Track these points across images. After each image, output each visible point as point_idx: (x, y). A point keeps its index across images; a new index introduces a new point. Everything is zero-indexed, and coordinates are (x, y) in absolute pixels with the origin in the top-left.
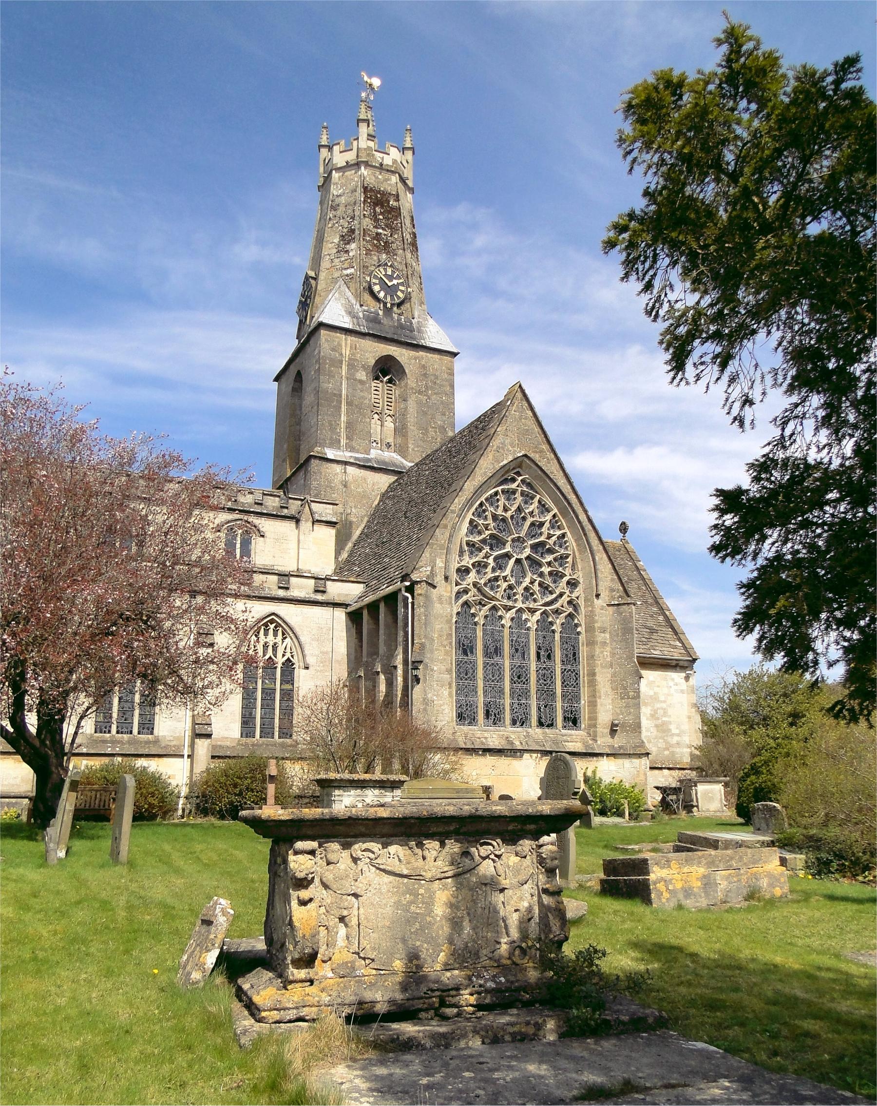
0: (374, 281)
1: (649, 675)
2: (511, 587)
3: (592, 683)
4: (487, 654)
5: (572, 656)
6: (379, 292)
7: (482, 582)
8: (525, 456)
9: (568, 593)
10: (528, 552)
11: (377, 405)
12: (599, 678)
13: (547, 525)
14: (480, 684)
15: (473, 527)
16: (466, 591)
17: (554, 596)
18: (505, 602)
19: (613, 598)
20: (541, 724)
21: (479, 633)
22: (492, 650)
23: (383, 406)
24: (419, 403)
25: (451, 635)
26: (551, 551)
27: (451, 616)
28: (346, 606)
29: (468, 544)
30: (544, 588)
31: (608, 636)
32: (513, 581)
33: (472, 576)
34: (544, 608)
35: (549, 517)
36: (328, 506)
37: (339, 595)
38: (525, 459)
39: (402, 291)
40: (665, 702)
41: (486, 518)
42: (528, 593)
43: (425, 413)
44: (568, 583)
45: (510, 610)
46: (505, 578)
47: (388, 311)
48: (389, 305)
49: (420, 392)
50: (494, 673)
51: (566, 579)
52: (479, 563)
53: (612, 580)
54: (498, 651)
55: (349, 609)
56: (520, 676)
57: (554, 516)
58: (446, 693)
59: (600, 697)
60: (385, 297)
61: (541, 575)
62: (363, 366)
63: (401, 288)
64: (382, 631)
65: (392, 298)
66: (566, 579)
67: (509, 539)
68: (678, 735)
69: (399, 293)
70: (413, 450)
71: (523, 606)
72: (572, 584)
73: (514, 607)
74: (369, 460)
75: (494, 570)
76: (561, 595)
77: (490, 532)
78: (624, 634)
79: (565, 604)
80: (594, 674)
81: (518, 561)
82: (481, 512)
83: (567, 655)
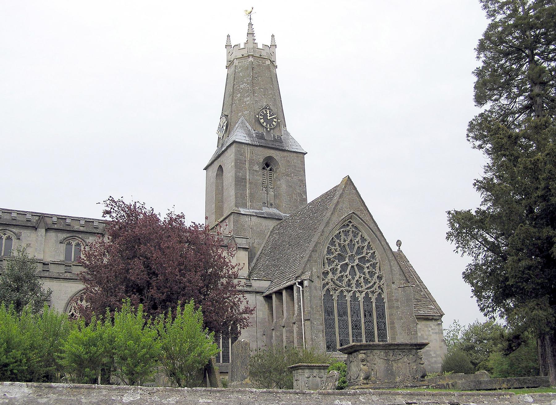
0: (261, 117)
1: (421, 325)
2: (349, 280)
3: (393, 328)
4: (339, 315)
5: (381, 316)
6: (263, 123)
7: (335, 278)
8: (353, 213)
9: (378, 282)
10: (357, 262)
11: (265, 183)
12: (396, 325)
13: (366, 248)
15: (329, 252)
16: (327, 284)
17: (371, 284)
18: (347, 288)
19: (401, 284)
21: (335, 305)
23: (268, 183)
25: (322, 306)
26: (368, 261)
27: (322, 296)
28: (263, 293)
30: (366, 281)
31: (399, 303)
32: (350, 277)
33: (330, 275)
34: (367, 290)
35: (366, 244)
36: (244, 239)
37: (258, 287)
38: (354, 214)
40: (427, 339)
41: (335, 246)
42: (358, 284)
43: (291, 187)
44: (378, 277)
45: (350, 292)
46: (346, 276)
47: (268, 132)
48: (269, 129)
49: (287, 175)
51: (376, 275)
52: (333, 268)
53: (400, 275)
54: (345, 313)
55: (264, 294)
56: (356, 326)
57: (369, 243)
58: (321, 335)
61: (364, 273)
62: (257, 163)
63: (275, 120)
64: (285, 306)
65: (270, 126)
66: (376, 275)
67: (348, 256)
68: (435, 357)
69: (274, 123)
70: (285, 206)
71: (356, 290)
72: (380, 278)
73: (352, 290)
74: (263, 213)
75: (341, 272)
76: (375, 283)
77: (338, 253)
78: (407, 302)
79: (377, 288)
80: (394, 323)
81: (352, 267)
82: (333, 243)
83: (379, 314)
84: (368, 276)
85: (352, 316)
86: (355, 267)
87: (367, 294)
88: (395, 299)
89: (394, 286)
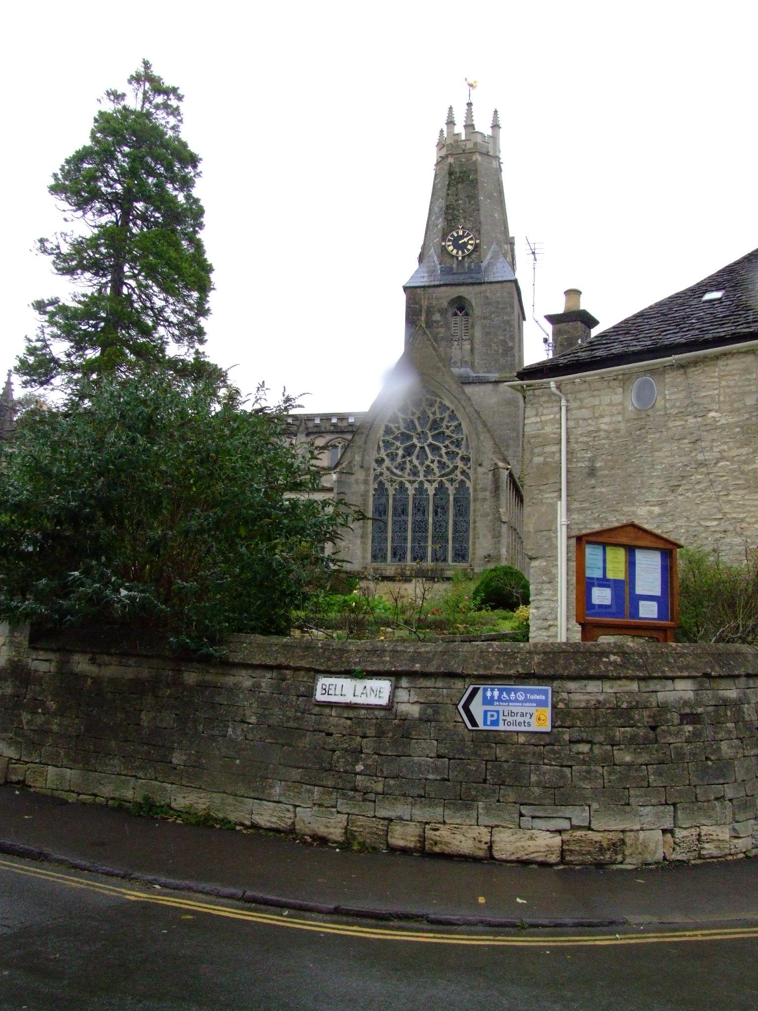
0: (448, 243)
6: (452, 251)
14: (390, 535)
20: (414, 559)
22: (400, 510)
24: (484, 327)
29: (384, 441)
30: (442, 465)
34: (439, 479)
39: (471, 245)
42: (429, 471)
43: (488, 334)
48: (460, 258)
49: (485, 318)
50: (400, 528)
51: (460, 455)
54: (404, 512)
58: (359, 542)
59: (479, 538)
60: (457, 253)
63: (471, 242)
65: (463, 252)
66: (460, 455)
70: (478, 363)
81: (430, 445)
83: (459, 510)
84: (445, 459)
85: (414, 515)
86: (427, 448)
87: (441, 484)
88: (482, 488)
89: (480, 470)
